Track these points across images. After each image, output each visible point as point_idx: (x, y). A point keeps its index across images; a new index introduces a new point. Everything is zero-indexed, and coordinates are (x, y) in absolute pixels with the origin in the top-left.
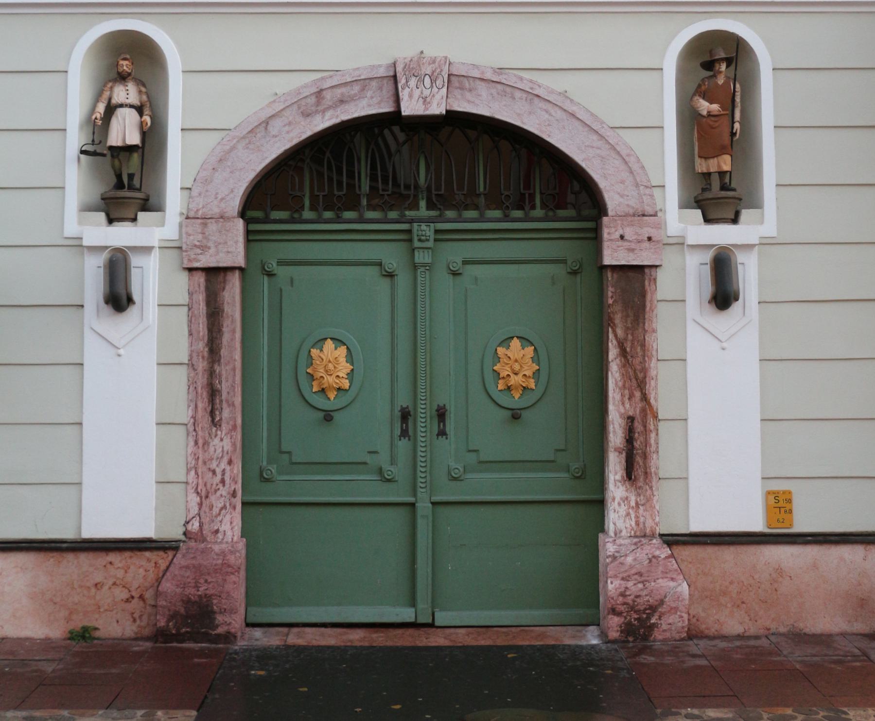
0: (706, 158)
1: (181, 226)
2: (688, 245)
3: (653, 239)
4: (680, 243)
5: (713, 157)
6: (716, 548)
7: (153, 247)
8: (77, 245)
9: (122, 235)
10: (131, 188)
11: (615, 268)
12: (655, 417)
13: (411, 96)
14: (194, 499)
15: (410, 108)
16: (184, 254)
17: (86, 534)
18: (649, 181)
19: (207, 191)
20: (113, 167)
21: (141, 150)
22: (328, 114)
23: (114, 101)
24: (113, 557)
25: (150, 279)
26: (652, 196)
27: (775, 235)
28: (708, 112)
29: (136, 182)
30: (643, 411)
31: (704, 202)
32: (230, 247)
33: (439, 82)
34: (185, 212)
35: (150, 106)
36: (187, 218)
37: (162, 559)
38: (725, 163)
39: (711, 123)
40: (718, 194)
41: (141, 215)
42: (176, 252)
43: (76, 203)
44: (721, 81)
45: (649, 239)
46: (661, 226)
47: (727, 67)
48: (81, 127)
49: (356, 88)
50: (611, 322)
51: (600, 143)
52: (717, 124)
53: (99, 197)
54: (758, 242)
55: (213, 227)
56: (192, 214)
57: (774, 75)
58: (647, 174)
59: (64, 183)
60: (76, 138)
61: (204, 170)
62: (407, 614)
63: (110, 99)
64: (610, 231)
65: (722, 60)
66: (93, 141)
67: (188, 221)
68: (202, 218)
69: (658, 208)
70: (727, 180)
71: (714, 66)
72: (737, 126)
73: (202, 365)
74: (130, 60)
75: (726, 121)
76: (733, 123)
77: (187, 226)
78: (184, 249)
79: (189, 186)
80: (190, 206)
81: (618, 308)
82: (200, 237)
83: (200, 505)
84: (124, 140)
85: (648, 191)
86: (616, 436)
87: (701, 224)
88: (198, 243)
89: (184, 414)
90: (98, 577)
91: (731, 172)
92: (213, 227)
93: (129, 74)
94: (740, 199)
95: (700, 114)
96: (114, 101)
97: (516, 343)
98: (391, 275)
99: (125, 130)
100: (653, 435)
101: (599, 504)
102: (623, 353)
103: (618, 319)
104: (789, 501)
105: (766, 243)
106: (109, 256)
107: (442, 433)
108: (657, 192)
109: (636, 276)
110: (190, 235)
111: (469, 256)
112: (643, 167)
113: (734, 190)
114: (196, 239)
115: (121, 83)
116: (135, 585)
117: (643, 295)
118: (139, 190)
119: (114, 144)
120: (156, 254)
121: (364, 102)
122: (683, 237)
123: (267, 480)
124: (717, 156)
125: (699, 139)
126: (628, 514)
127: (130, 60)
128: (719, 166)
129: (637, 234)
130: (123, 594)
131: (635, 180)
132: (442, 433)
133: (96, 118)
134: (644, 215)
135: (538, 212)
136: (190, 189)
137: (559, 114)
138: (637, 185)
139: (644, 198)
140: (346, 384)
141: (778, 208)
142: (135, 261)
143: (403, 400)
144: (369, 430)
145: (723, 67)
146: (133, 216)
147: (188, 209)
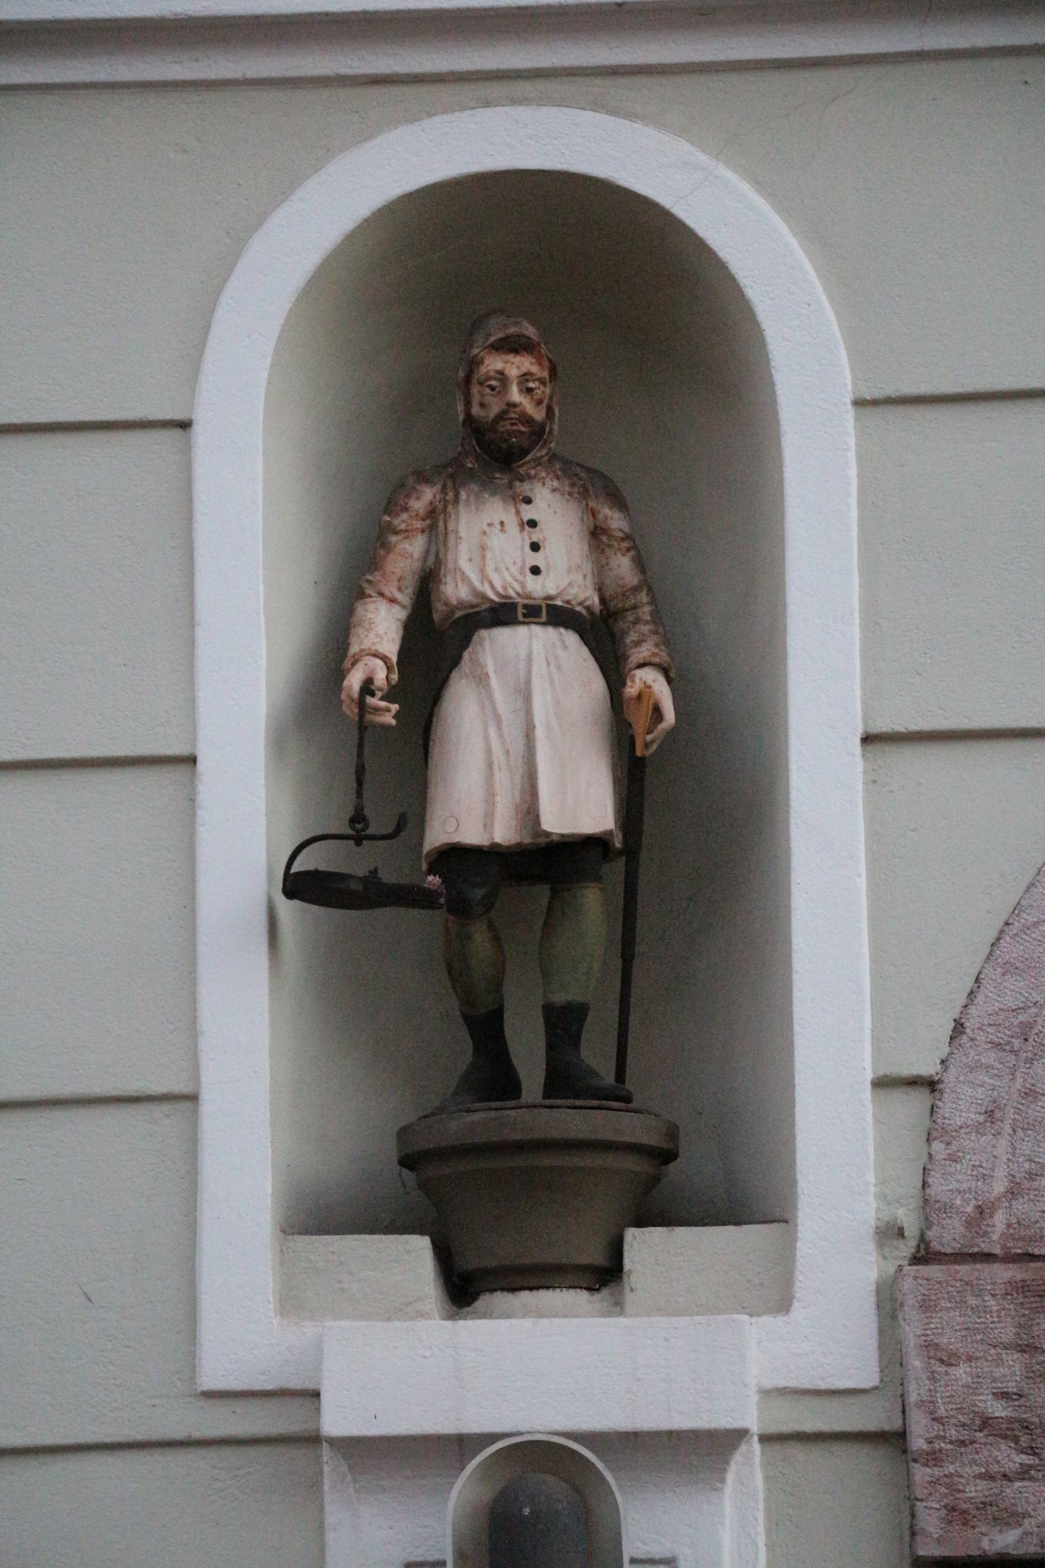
1: (888, 1304)
7: (741, 1434)
8: (283, 1437)
9: (541, 1367)
10: (564, 1082)
16: (921, 1474)
19: (1030, 1094)
20: (457, 971)
21: (616, 869)
23: (455, 591)
29: (596, 1053)
34: (908, 1218)
35: (657, 617)
36: (925, 1255)
41: (643, 1246)
42: (860, 1469)
43: (268, 1187)
48: (278, 744)
53: (390, 1151)
56: (949, 1234)
59: (196, 1078)
60: (246, 814)
61: (1010, 969)
63: (427, 582)
66: (358, 818)
67: (934, 1271)
68: (1010, 1258)
74: (540, 348)
77: (927, 1306)
78: (917, 1443)
79: (928, 1068)
80: (939, 1188)
82: (1011, 1369)
84: (529, 810)
88: (999, 1410)
93: (538, 433)
96: (455, 591)
99: (527, 751)
106: (486, 1493)
110: (949, 1361)
115: (488, 485)
118: (618, 1096)
119: (472, 835)
127: (540, 348)
133: (367, 688)
136: (931, 1085)
146: (596, 1256)
147: (928, 1206)
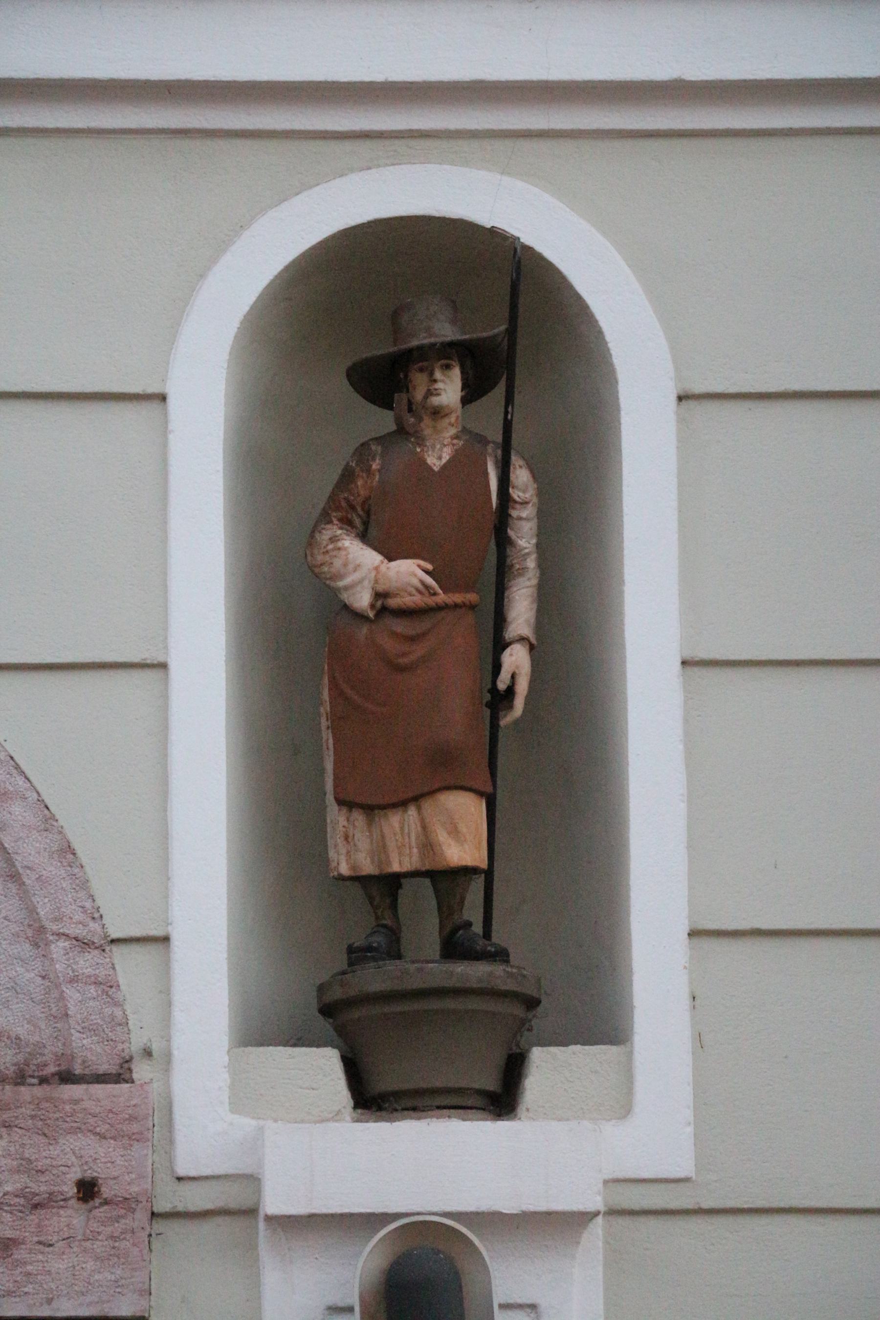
0: (370, 810)
2: (269, 1219)
3: (106, 1191)
4: (237, 1212)
5: (403, 804)
18: (96, 916)
26: (108, 987)
27: (682, 1164)
28: (378, 595)
31: (356, 1014)
38: (454, 832)
39: (388, 644)
44: (438, 455)
45: (87, 1190)
46: (144, 1127)
47: (472, 392)
52: (419, 651)
54: (594, 1201)
57: (681, 421)
58: (84, 885)
65: (447, 352)
69: (137, 1041)
70: (473, 913)
71: (404, 386)
72: (516, 660)
75: (461, 638)
76: (500, 645)
85: (86, 963)
87: (336, 1116)
91: (489, 874)
94: (532, 1003)
95: (346, 607)
105: (638, 1207)
108: (130, 968)
112: (68, 851)
113: (501, 955)
122: (252, 1180)
124: (416, 799)
125: (337, 722)
128: (428, 846)
129: (26, 1166)
131: (32, 911)
134: (67, 1077)
138: (38, 936)
139: (72, 994)
141: (699, 1040)
145: (449, 389)
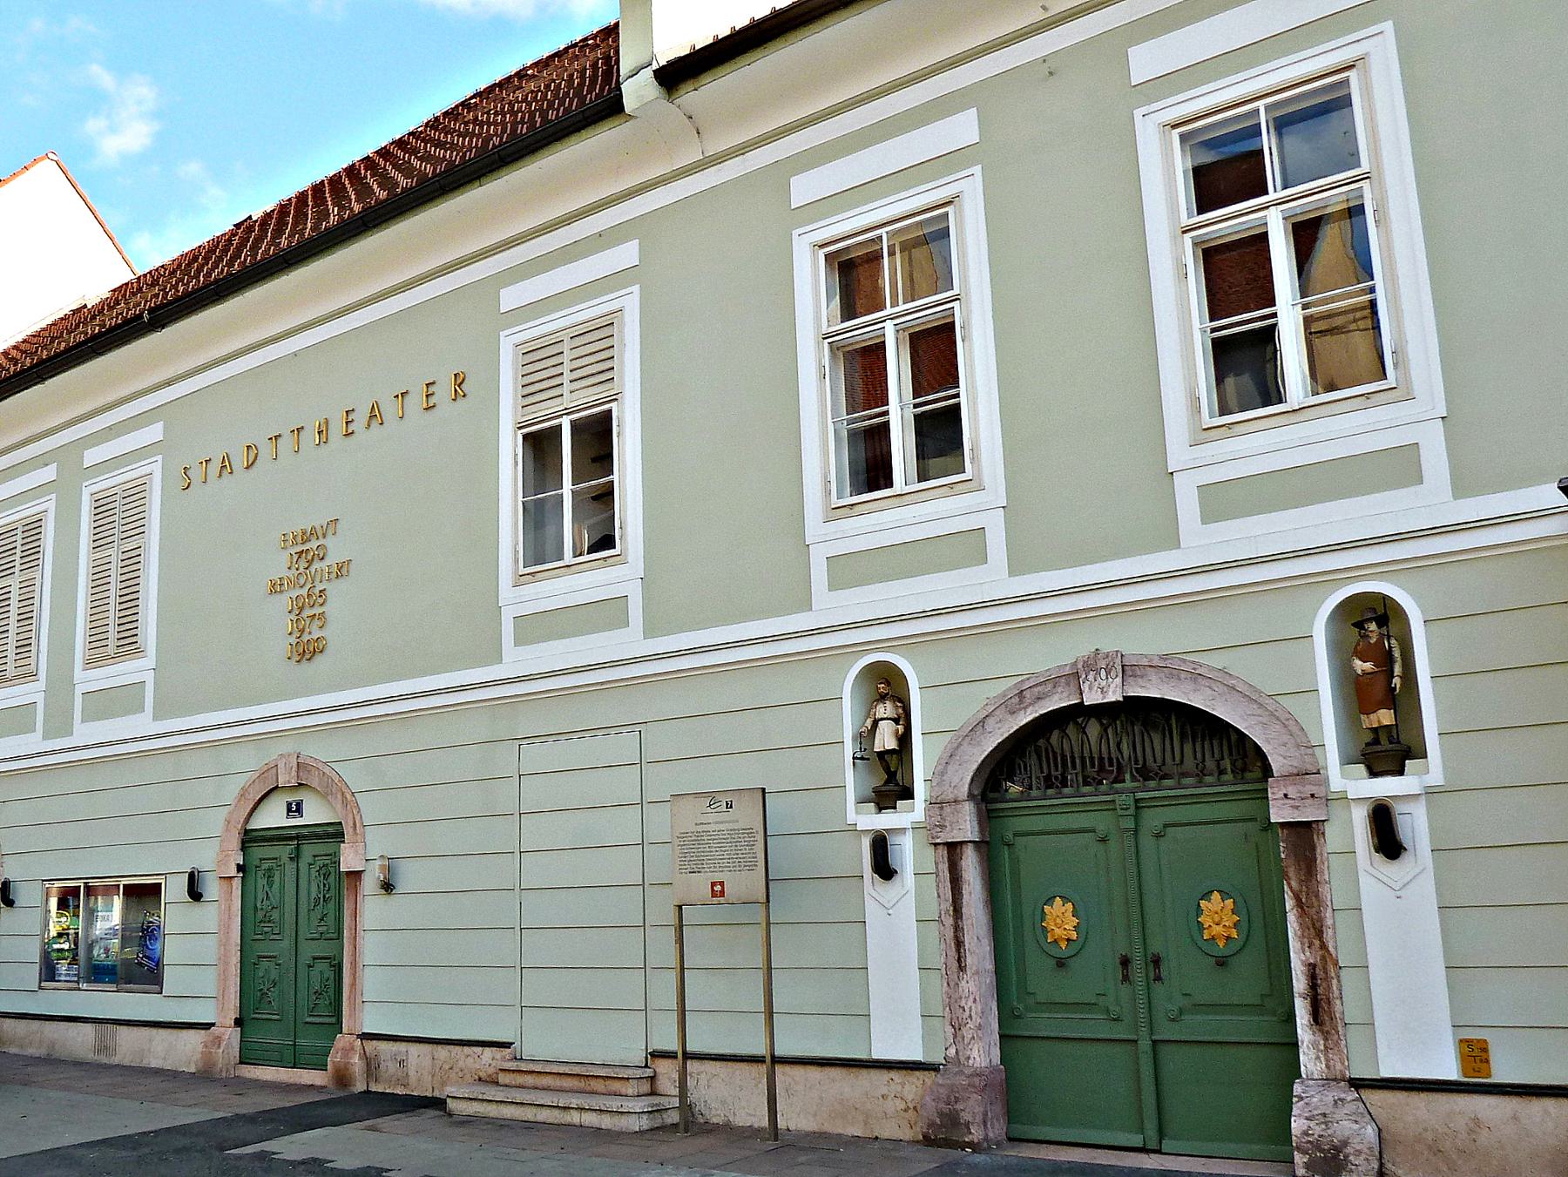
6: (1405, 1094)
11: (1283, 825)
12: (1336, 963)
13: (1090, 688)
14: (950, 1030)
15: (1091, 698)
17: (875, 1056)
22: (1029, 711)
24: (893, 1074)
25: (906, 853)
26: (1313, 755)
30: (1323, 958)
32: (965, 826)
33: (1113, 674)
37: (929, 1077)
40: (1388, 751)
49: (1049, 686)
50: (1285, 876)
51: (1259, 712)
55: (948, 809)
60: (849, 749)
62: (1137, 1140)
64: (1275, 792)
72: (1396, 681)
73: (949, 921)
81: (1291, 861)
83: (955, 1036)
86: (1300, 983)
89: (939, 961)
90: (884, 1091)
92: (948, 809)
97: (1216, 896)
98: (1103, 840)
100: (1335, 982)
101: (1295, 1045)
102: (1299, 903)
103: (1292, 872)
104: (1485, 1050)
105: (1430, 792)
107: (1158, 978)
109: (1304, 834)
111: (1169, 820)
114: (936, 820)
116: (910, 1097)
117: (1313, 848)
120: (909, 834)
121: (1056, 697)
123: (1019, 1017)
126: (1318, 1058)
130: (901, 1105)
132: (1158, 978)
135: (1229, 777)
137: (1221, 688)
138: (1298, 746)
140: (1074, 935)
142: (891, 840)
143: (1123, 950)
144: (1094, 976)
